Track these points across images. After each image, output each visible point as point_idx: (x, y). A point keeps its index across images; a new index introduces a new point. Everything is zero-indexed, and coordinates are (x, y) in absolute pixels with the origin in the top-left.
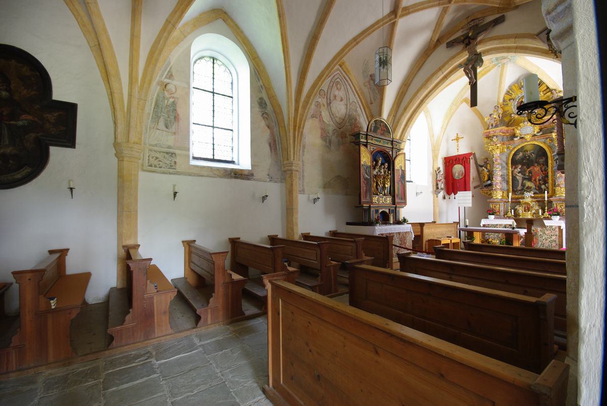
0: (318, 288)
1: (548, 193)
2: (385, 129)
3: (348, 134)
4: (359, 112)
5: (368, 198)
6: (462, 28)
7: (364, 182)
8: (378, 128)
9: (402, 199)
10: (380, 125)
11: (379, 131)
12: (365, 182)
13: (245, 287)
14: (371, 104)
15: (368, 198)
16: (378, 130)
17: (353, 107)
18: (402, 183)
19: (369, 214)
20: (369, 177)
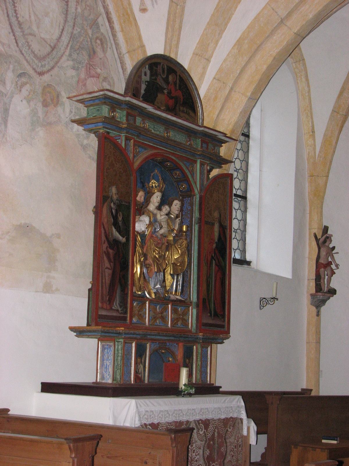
0: (123, 240)
1: (190, 375)
2: (179, 94)
3: (64, 95)
4: (102, 30)
5: (116, 305)
6: (79, 331)
7: (108, 255)
8: (160, 90)
9: (216, 315)
10: (166, 81)
11: (161, 97)
12: (111, 251)
13: (331, 247)
14: (144, 10)
15: (116, 305)
16: (160, 96)
17: (86, 13)
18: (219, 265)
19: (172, 317)
20: (123, 240)
